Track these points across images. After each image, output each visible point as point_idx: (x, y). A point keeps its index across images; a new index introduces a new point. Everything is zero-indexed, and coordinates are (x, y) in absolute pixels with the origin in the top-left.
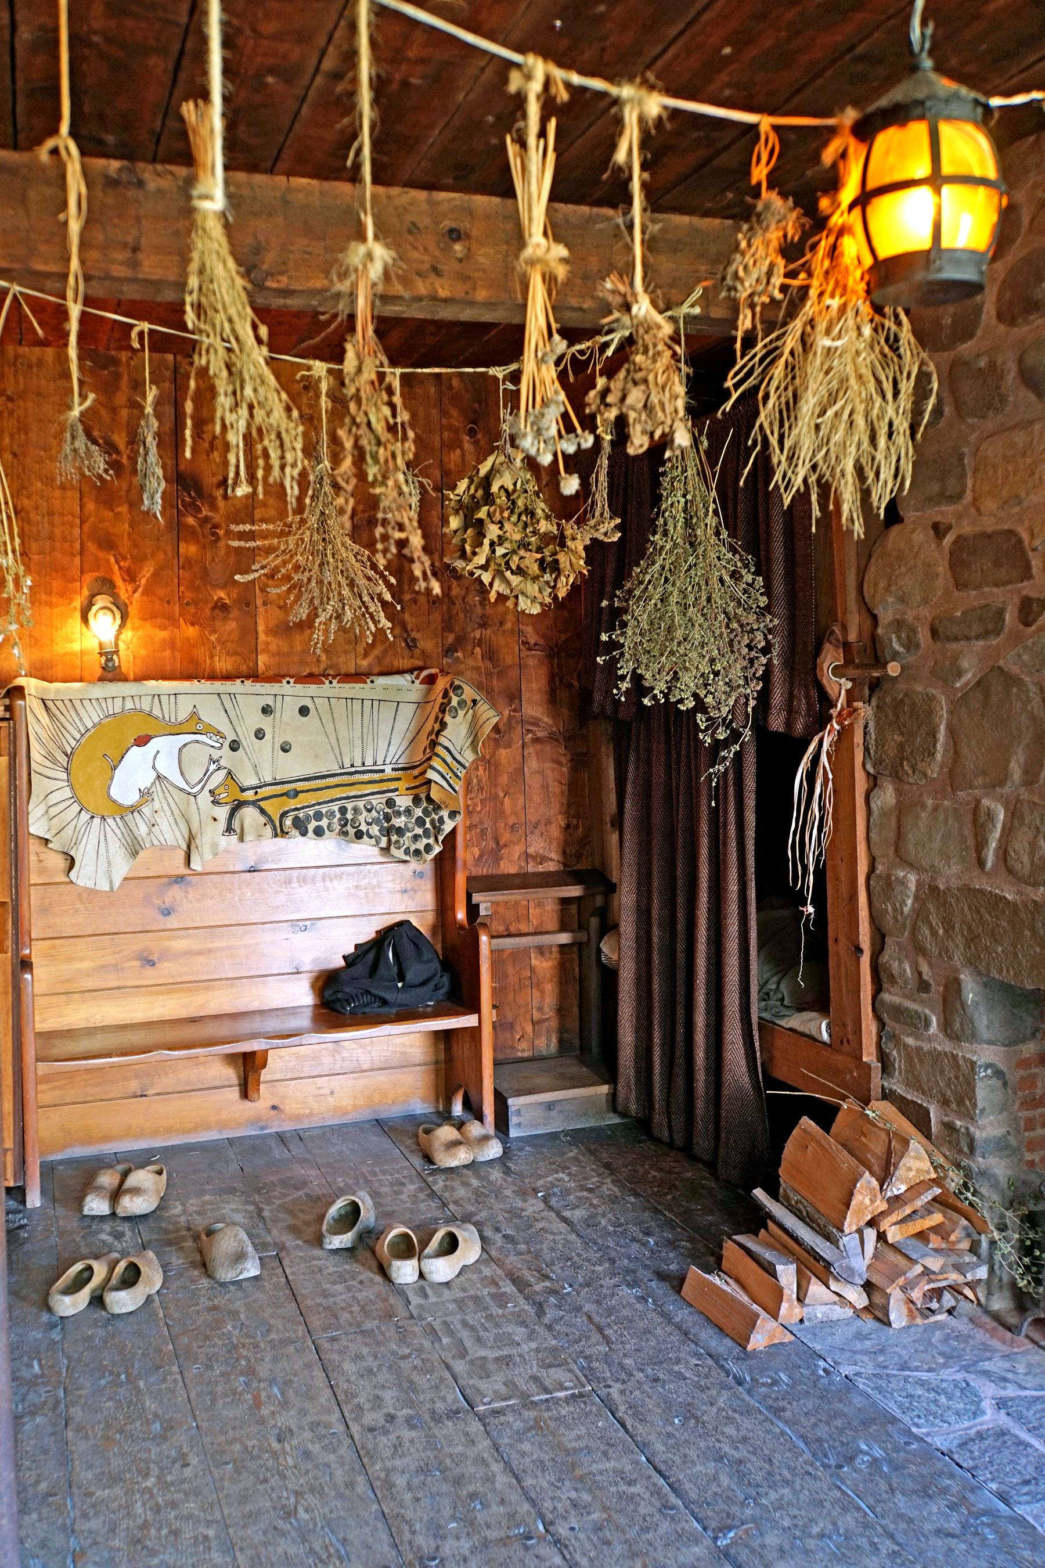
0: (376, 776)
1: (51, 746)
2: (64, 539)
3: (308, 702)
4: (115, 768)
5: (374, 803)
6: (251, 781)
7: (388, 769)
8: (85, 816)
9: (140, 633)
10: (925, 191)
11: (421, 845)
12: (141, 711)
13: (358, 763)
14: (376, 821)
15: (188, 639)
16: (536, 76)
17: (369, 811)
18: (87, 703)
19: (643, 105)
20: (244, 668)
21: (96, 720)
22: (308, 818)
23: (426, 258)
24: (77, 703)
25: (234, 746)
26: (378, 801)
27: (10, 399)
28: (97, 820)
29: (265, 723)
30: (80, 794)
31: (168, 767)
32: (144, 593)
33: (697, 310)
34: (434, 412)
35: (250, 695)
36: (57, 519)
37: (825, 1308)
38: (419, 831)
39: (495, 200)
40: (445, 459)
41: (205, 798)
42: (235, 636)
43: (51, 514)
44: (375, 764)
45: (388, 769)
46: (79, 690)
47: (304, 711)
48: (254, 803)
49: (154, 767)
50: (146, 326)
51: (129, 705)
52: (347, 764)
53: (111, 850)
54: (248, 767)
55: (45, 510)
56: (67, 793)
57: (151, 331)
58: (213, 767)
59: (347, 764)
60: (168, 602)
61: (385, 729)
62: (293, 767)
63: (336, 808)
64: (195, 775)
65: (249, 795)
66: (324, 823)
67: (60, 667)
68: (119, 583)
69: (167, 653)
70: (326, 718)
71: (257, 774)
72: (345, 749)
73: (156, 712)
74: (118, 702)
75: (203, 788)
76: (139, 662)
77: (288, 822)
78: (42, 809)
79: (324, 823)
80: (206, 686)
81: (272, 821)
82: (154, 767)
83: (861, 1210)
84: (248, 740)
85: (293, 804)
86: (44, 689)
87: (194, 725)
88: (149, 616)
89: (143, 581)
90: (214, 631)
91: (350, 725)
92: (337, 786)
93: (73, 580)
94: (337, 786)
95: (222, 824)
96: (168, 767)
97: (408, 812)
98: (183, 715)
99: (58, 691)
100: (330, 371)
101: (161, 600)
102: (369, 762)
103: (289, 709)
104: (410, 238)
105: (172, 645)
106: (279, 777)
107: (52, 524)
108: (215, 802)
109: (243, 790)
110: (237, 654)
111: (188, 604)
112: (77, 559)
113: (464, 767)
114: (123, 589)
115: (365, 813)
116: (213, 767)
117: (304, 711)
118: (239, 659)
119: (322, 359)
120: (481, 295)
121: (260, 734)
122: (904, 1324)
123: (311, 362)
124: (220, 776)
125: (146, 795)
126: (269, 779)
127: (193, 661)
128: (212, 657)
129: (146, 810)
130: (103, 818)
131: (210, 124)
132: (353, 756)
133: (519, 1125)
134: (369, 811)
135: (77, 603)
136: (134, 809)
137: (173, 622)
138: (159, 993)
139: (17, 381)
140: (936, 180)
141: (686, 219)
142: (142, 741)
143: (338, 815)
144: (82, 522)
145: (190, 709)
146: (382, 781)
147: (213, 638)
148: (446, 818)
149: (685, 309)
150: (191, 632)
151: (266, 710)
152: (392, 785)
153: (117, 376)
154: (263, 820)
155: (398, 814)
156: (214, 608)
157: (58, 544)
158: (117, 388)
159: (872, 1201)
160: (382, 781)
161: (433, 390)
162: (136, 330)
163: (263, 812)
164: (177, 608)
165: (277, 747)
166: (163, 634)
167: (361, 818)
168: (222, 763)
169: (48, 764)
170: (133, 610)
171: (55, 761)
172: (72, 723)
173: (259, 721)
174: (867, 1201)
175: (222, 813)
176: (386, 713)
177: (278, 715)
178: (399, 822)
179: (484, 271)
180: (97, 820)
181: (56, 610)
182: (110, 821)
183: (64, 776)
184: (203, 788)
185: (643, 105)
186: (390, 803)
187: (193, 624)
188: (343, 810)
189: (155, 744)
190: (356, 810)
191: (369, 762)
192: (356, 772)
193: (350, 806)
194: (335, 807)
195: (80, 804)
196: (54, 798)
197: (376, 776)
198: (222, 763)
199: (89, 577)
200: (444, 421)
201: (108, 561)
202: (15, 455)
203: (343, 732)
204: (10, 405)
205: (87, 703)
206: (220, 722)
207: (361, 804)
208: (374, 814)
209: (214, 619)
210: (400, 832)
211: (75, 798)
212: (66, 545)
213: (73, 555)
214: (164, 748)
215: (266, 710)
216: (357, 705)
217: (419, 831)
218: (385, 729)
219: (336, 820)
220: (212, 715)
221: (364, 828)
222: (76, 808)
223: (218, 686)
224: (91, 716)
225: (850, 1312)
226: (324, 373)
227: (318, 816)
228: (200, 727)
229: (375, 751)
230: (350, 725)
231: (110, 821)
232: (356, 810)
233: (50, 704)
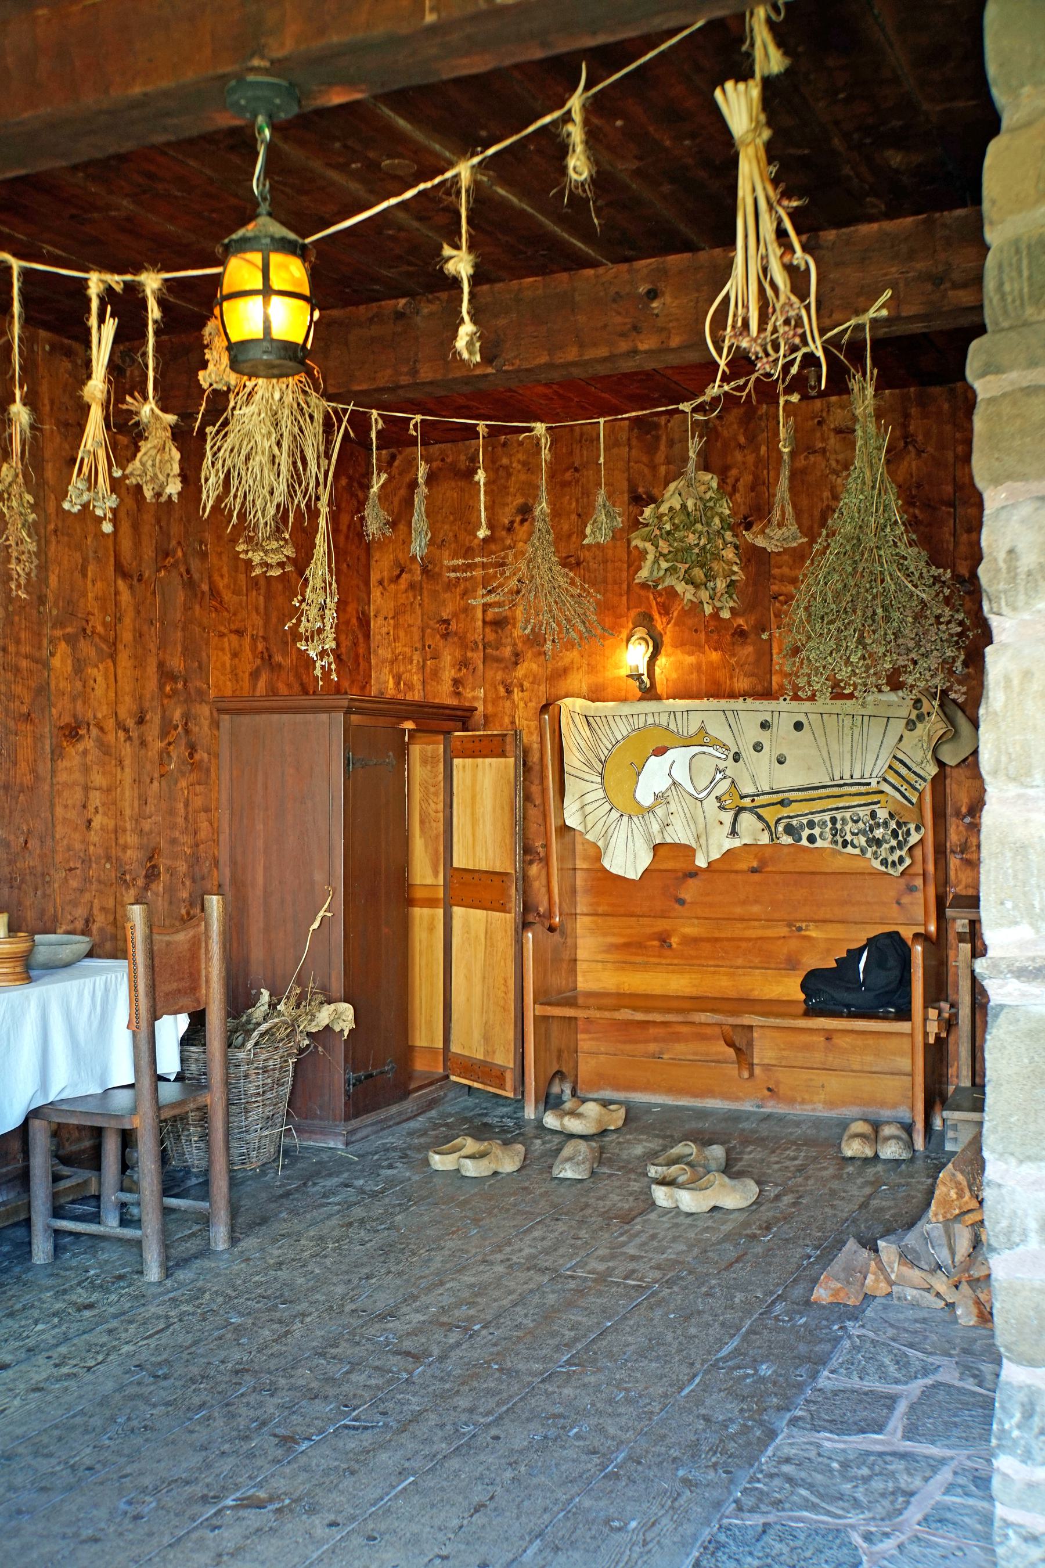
0: (863, 789)
1: (590, 754)
2: (615, 582)
3: (802, 718)
4: (639, 774)
5: (861, 814)
6: (748, 789)
7: (874, 782)
8: (615, 814)
9: (672, 659)
10: (260, 298)
11: (895, 857)
12: (660, 726)
13: (847, 776)
14: (863, 832)
15: (711, 663)
16: (96, 282)
17: (856, 822)
18: (617, 719)
19: (151, 282)
20: (759, 688)
21: (625, 733)
22: (802, 827)
23: (627, 320)
24: (610, 719)
25: (737, 758)
26: (864, 812)
27: (576, 470)
28: (625, 819)
29: (764, 737)
30: (611, 795)
31: (681, 775)
32: (676, 624)
33: (884, 313)
34: (948, 428)
35: (751, 712)
36: (610, 566)
37: (915, 1292)
38: (894, 843)
39: (687, 256)
40: (959, 474)
41: (711, 804)
42: (751, 659)
43: (605, 561)
44: (862, 777)
45: (874, 782)
46: (612, 708)
47: (798, 726)
48: (751, 810)
49: (670, 774)
50: (419, 418)
51: (650, 720)
52: (837, 777)
53: (637, 844)
54: (747, 776)
55: (600, 559)
56: (600, 794)
57: (422, 421)
58: (719, 776)
59: (837, 777)
60: (696, 631)
61: (874, 744)
62: (789, 778)
63: (828, 818)
64: (703, 782)
65: (747, 802)
66: (816, 831)
67: (610, 690)
68: (656, 616)
69: (694, 676)
70: (819, 732)
71: (755, 783)
72: (836, 762)
73: (672, 727)
74: (642, 717)
75: (709, 794)
76: (670, 684)
77: (780, 829)
78: (577, 805)
79: (816, 831)
80: (713, 703)
81: (769, 827)
82: (670, 774)
83: (946, 1202)
84: (747, 753)
85: (785, 812)
86: (588, 708)
87: (701, 738)
88: (680, 644)
89: (675, 614)
90: (733, 655)
91: (840, 741)
92: (829, 797)
93: (621, 616)
94: (829, 797)
95: (727, 827)
96: (681, 775)
97: (886, 824)
98: (693, 730)
99: (597, 709)
100: (548, 429)
101: (690, 629)
102: (857, 775)
103: (785, 724)
104: (614, 306)
105: (698, 668)
106: (776, 787)
107: (605, 570)
108: (722, 808)
109: (742, 797)
110: (753, 675)
111: (712, 632)
112: (625, 598)
113: (925, 780)
114: (659, 623)
115: (850, 824)
116: (719, 776)
117: (798, 726)
118: (754, 680)
119: (542, 421)
120: (675, 342)
121: (758, 747)
122: (972, 1323)
123: (533, 425)
124: (725, 785)
125: (660, 798)
126: (766, 789)
127: (717, 683)
128: (731, 678)
129: (660, 811)
130: (630, 816)
131: (154, 312)
132: (843, 769)
133: (955, 1139)
134: (856, 822)
135: (624, 635)
136: (650, 810)
137: (699, 647)
138: (673, 972)
139: (582, 455)
140: (267, 291)
141: (875, 226)
142: (660, 751)
143: (830, 825)
144: (629, 567)
145: (699, 724)
146: (868, 793)
147: (733, 661)
148: (913, 831)
149: (872, 313)
150: (715, 656)
151: (765, 725)
152: (875, 798)
153: (657, 438)
154: (760, 825)
155: (878, 825)
156: (733, 635)
157: (610, 587)
158: (657, 448)
159: (960, 1195)
160: (868, 793)
161: (946, 406)
162: (413, 422)
163: (760, 818)
164: (703, 636)
165: (774, 759)
166: (691, 660)
167: (847, 828)
168: (728, 772)
169: (586, 769)
170: (667, 639)
171: (591, 766)
172: (607, 736)
173: (755, 734)
174: (953, 1194)
175: (728, 817)
176: (876, 728)
177: (775, 729)
178: (879, 833)
179: (677, 320)
180: (625, 819)
181: (607, 642)
182: (635, 819)
183: (599, 780)
184: (709, 794)
185: (151, 282)
186: (873, 815)
187: (716, 650)
188: (834, 820)
189: (671, 755)
190: (843, 820)
191: (857, 775)
192: (845, 785)
193: (839, 816)
194: (827, 817)
195: (611, 803)
196: (588, 798)
197: (863, 789)
198: (728, 772)
199: (633, 613)
200: (958, 435)
201: (648, 598)
202: (579, 515)
203: (834, 746)
204: (577, 475)
205: (617, 719)
206: (726, 737)
207: (847, 815)
208: (861, 825)
209: (733, 644)
210: (878, 843)
211: (606, 797)
212: (616, 587)
213: (621, 595)
214: (678, 756)
215: (765, 725)
216: (848, 721)
217: (894, 843)
218: (874, 744)
219: (828, 829)
220: (718, 730)
221: (849, 838)
222: (607, 807)
223: (724, 704)
224: (621, 730)
225: (942, 1304)
226: (543, 431)
227: (811, 825)
228: (707, 740)
229: (863, 765)
230: (840, 741)
231: (635, 819)
232: (843, 820)
233: (591, 719)
